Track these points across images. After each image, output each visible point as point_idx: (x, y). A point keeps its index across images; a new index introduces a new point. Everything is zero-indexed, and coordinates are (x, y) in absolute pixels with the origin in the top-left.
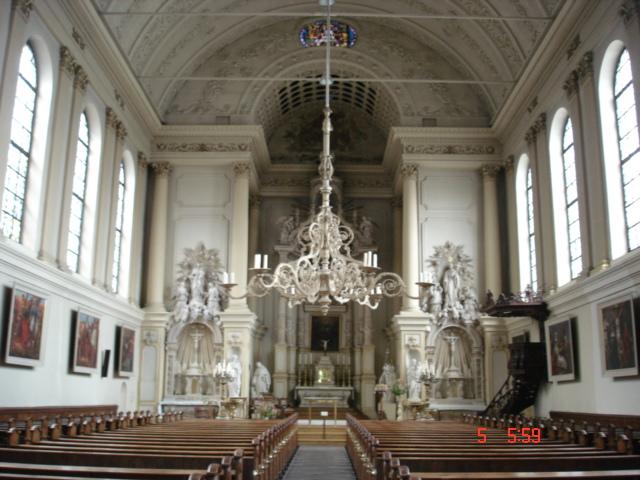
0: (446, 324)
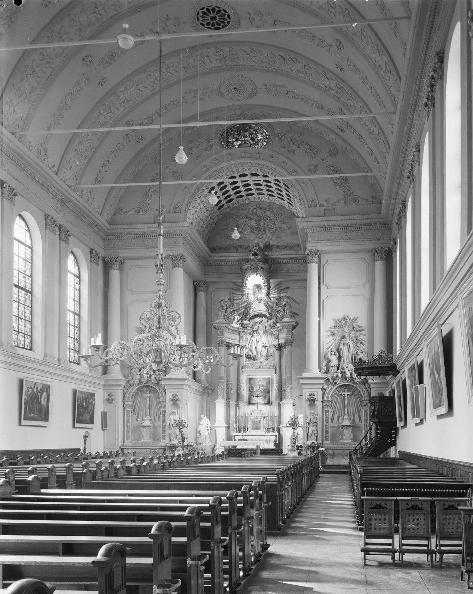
0: (340, 382)
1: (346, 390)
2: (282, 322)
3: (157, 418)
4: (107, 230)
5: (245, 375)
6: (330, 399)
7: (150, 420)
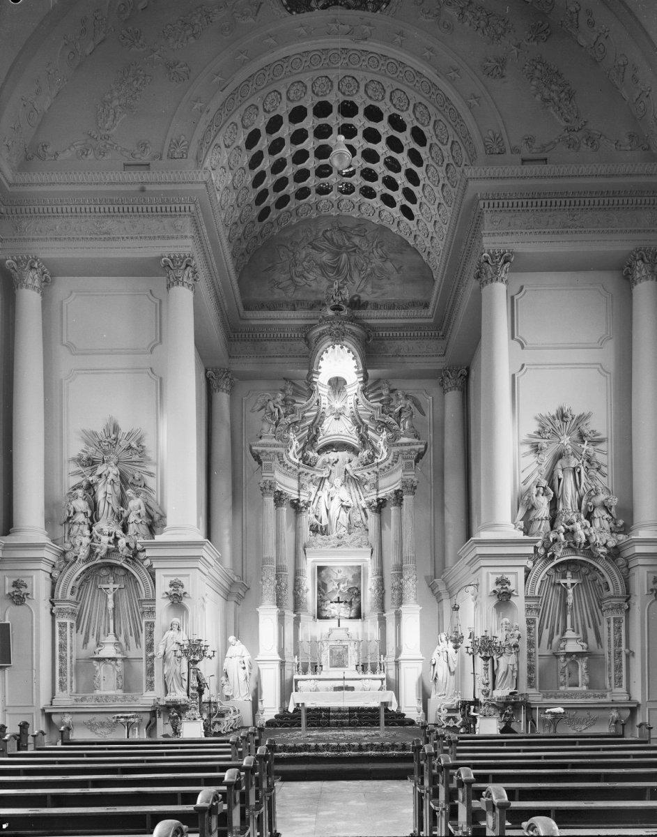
0: (561, 555)
1: (569, 574)
2: (398, 445)
3: (132, 640)
4: (7, 186)
5: (310, 560)
6: (536, 594)
7: (117, 644)
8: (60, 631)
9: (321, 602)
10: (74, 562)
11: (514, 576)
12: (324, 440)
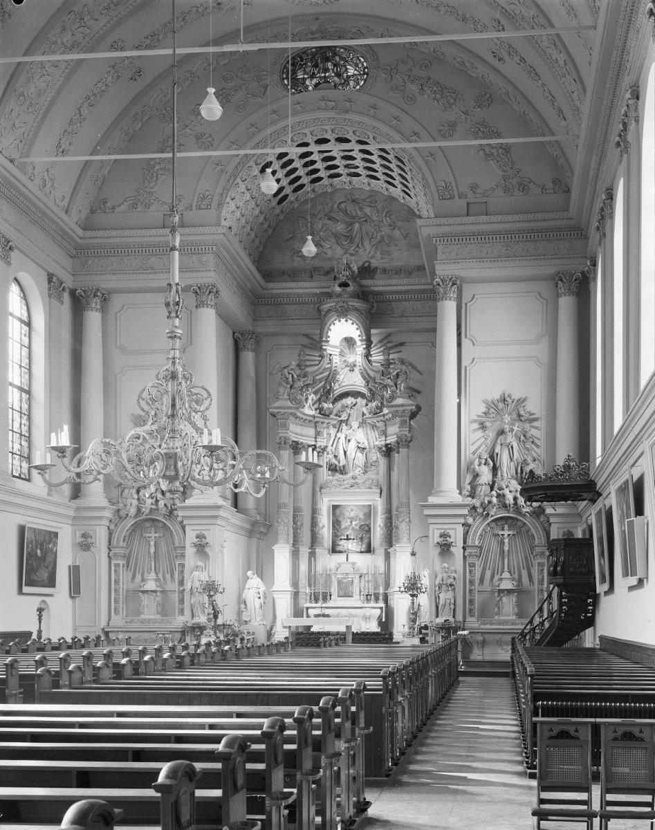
0: (495, 513)
1: (506, 527)
2: (392, 406)
3: (168, 576)
5: (326, 500)
7: (157, 580)
8: (115, 570)
9: (335, 537)
10: (125, 518)
11: (453, 531)
12: (339, 390)
